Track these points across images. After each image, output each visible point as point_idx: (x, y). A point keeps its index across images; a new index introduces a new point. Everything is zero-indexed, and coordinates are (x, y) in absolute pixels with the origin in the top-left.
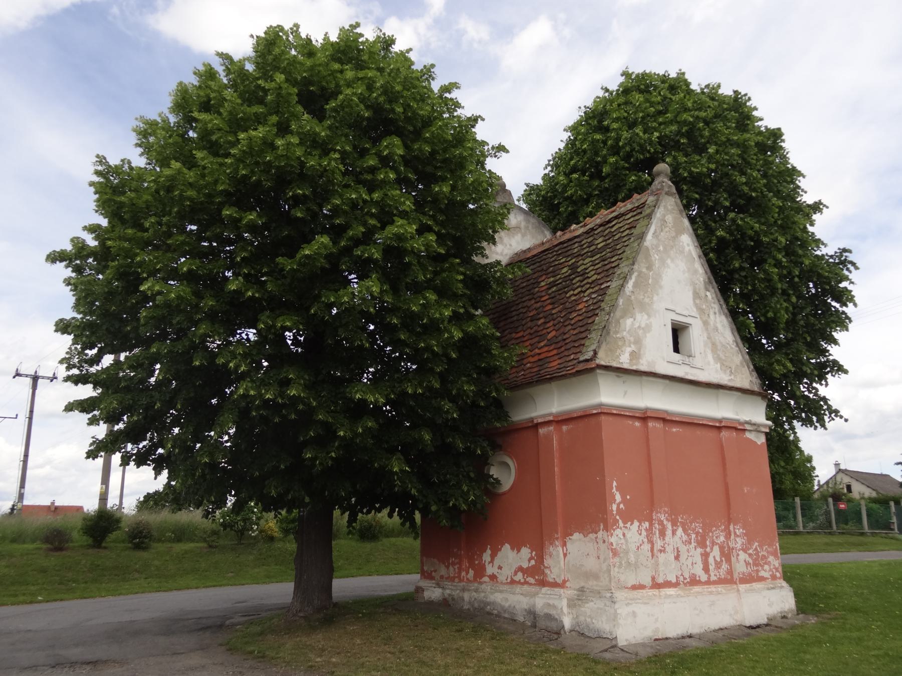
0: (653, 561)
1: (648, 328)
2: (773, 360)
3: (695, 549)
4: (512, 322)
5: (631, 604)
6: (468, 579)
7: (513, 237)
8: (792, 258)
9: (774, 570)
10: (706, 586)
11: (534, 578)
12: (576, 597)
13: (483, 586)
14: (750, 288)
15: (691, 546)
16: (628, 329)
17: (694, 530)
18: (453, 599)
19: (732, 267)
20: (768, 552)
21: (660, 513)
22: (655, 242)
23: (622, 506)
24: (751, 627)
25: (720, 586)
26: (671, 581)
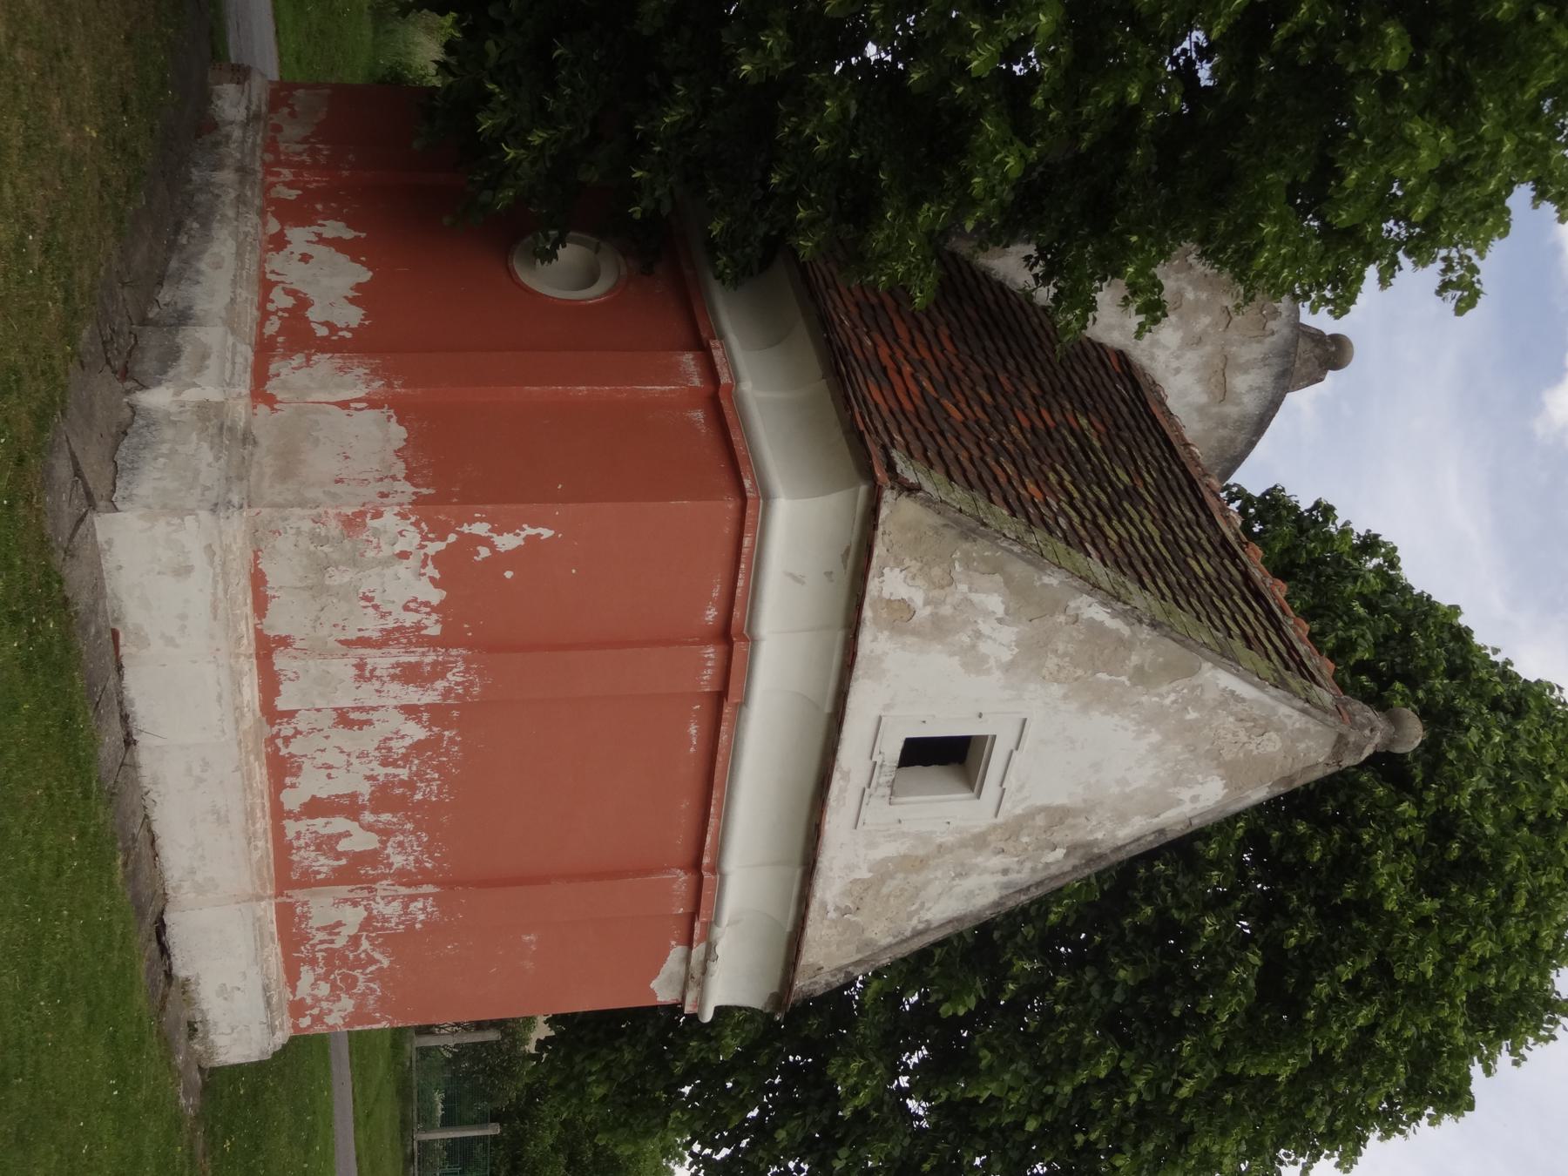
0: (332, 644)
1: (975, 662)
2: (873, 1059)
3: (369, 778)
4: (977, 334)
5: (211, 562)
6: (273, 185)
7: (1200, 381)
8: (1133, 1126)
9: (316, 1011)
10: (267, 805)
11: (279, 333)
12: (228, 423)
13: (254, 218)
14: (1059, 1008)
15: (375, 764)
16: (975, 597)
17: (420, 775)
18: (216, 144)
19: (1116, 961)
20: (364, 995)
21: (467, 671)
22: (1210, 696)
23: (484, 552)
24: (161, 928)
25: (270, 845)
26: (278, 693)
